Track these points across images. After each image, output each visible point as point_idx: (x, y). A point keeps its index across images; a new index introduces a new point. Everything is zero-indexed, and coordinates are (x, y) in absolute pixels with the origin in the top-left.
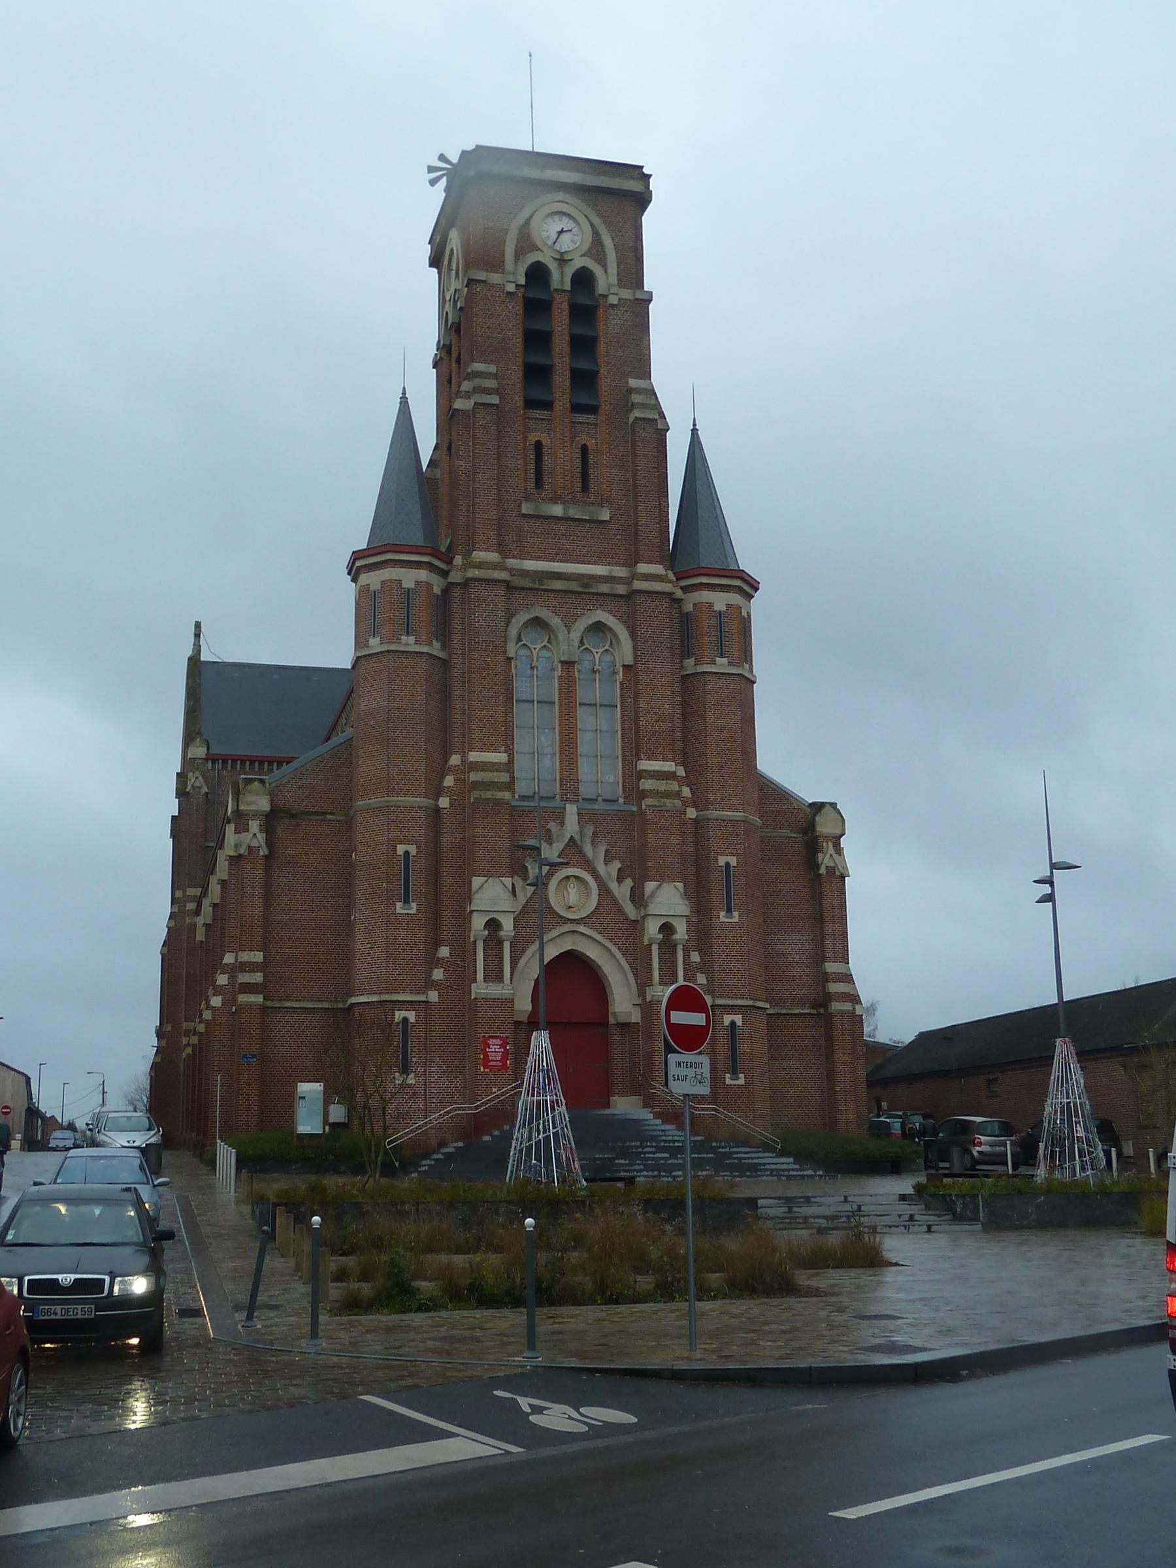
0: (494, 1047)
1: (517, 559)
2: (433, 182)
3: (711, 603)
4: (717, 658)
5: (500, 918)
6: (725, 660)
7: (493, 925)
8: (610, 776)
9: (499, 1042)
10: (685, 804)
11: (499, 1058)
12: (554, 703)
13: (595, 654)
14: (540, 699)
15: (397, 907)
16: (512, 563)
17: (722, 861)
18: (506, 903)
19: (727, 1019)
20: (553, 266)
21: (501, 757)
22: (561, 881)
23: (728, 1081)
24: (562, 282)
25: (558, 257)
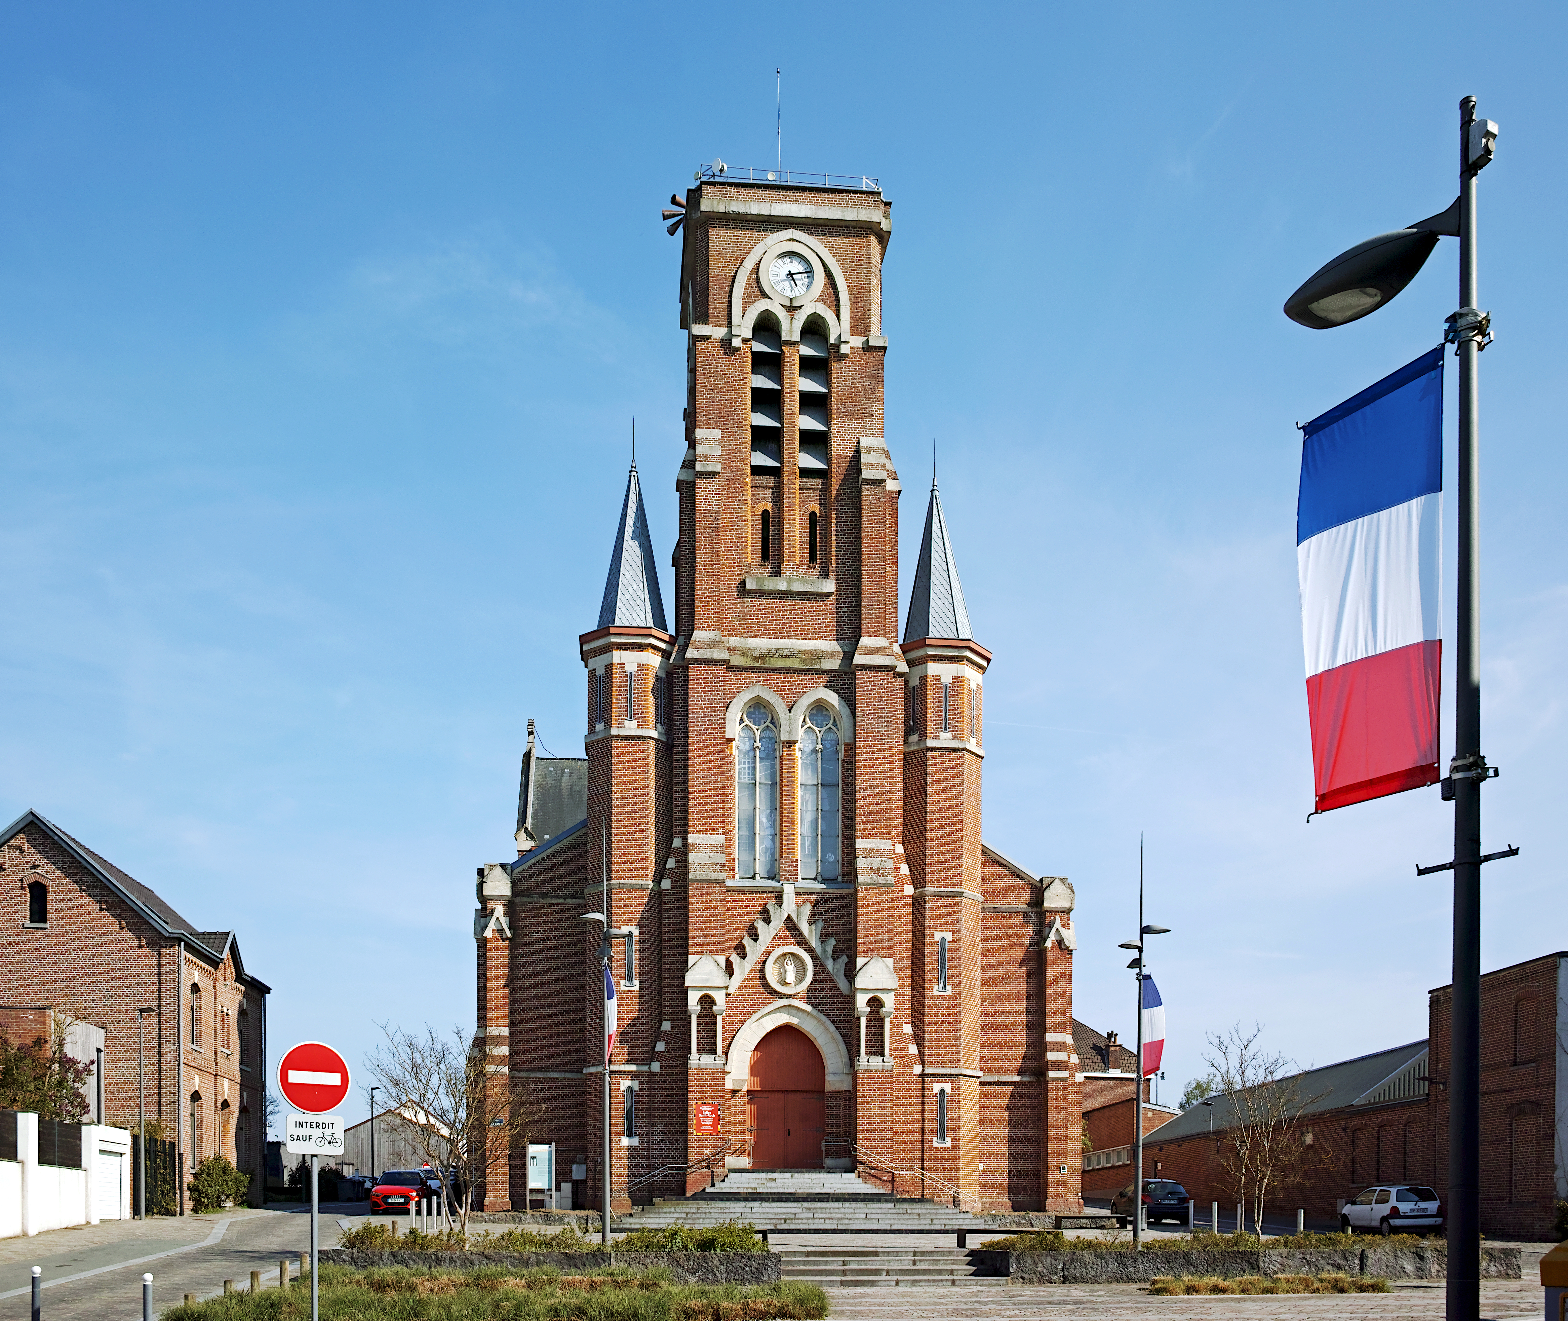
0: (705, 1113)
1: (740, 637)
2: (672, 231)
3: (936, 676)
4: (941, 733)
5: (882, 996)
6: (949, 735)
7: (875, 1003)
8: (830, 855)
9: (711, 1108)
10: (901, 880)
11: (711, 1123)
12: (801, 784)
13: (755, 730)
14: (804, 782)
15: (622, 985)
16: (733, 641)
17: (938, 936)
18: (720, 979)
19: (937, 1087)
20: (782, 315)
21: (720, 839)
22: (779, 957)
23: (935, 1144)
24: (791, 331)
25: (788, 304)
